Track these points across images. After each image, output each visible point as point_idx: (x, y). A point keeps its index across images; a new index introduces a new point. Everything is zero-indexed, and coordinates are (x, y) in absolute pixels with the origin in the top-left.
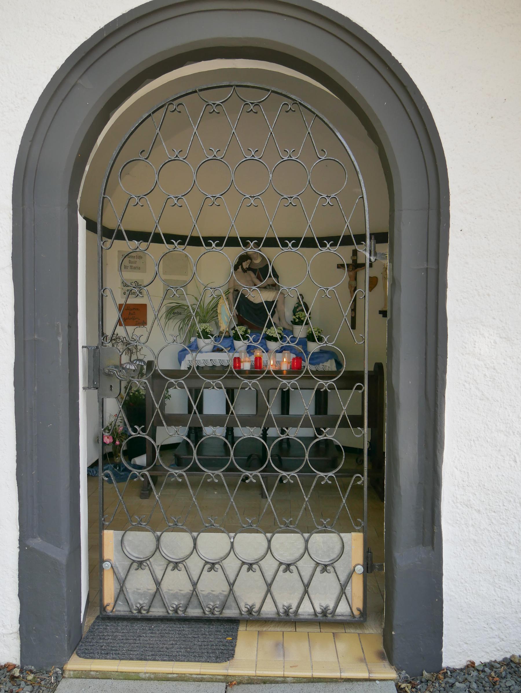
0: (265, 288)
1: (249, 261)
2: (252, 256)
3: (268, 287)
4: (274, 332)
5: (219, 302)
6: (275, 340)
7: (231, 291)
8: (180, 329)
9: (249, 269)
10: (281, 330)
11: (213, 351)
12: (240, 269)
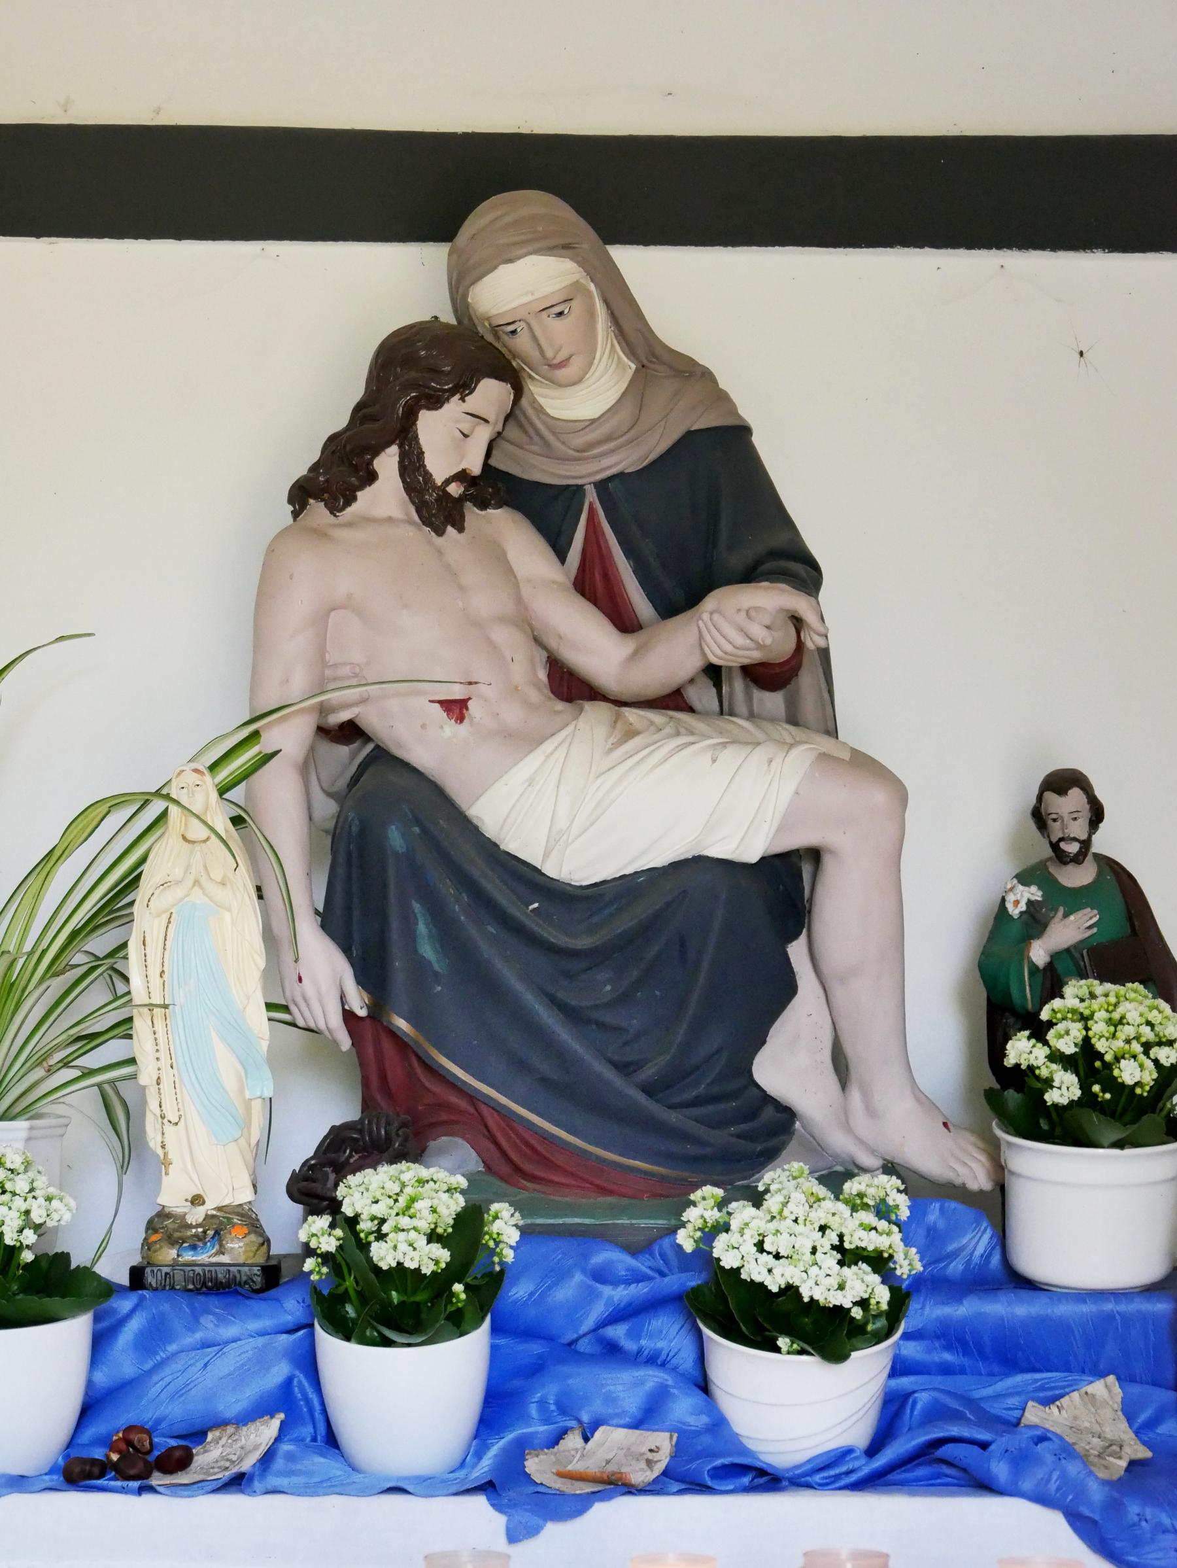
0: (673, 701)
1: (490, 394)
2: (522, 343)
3: (703, 696)
4: (782, 1234)
5: (151, 876)
6: (826, 1332)
7: (290, 737)
8: (609, 736)
9: (492, 486)
10: (883, 1211)
11: (78, 1472)
12: (385, 493)
